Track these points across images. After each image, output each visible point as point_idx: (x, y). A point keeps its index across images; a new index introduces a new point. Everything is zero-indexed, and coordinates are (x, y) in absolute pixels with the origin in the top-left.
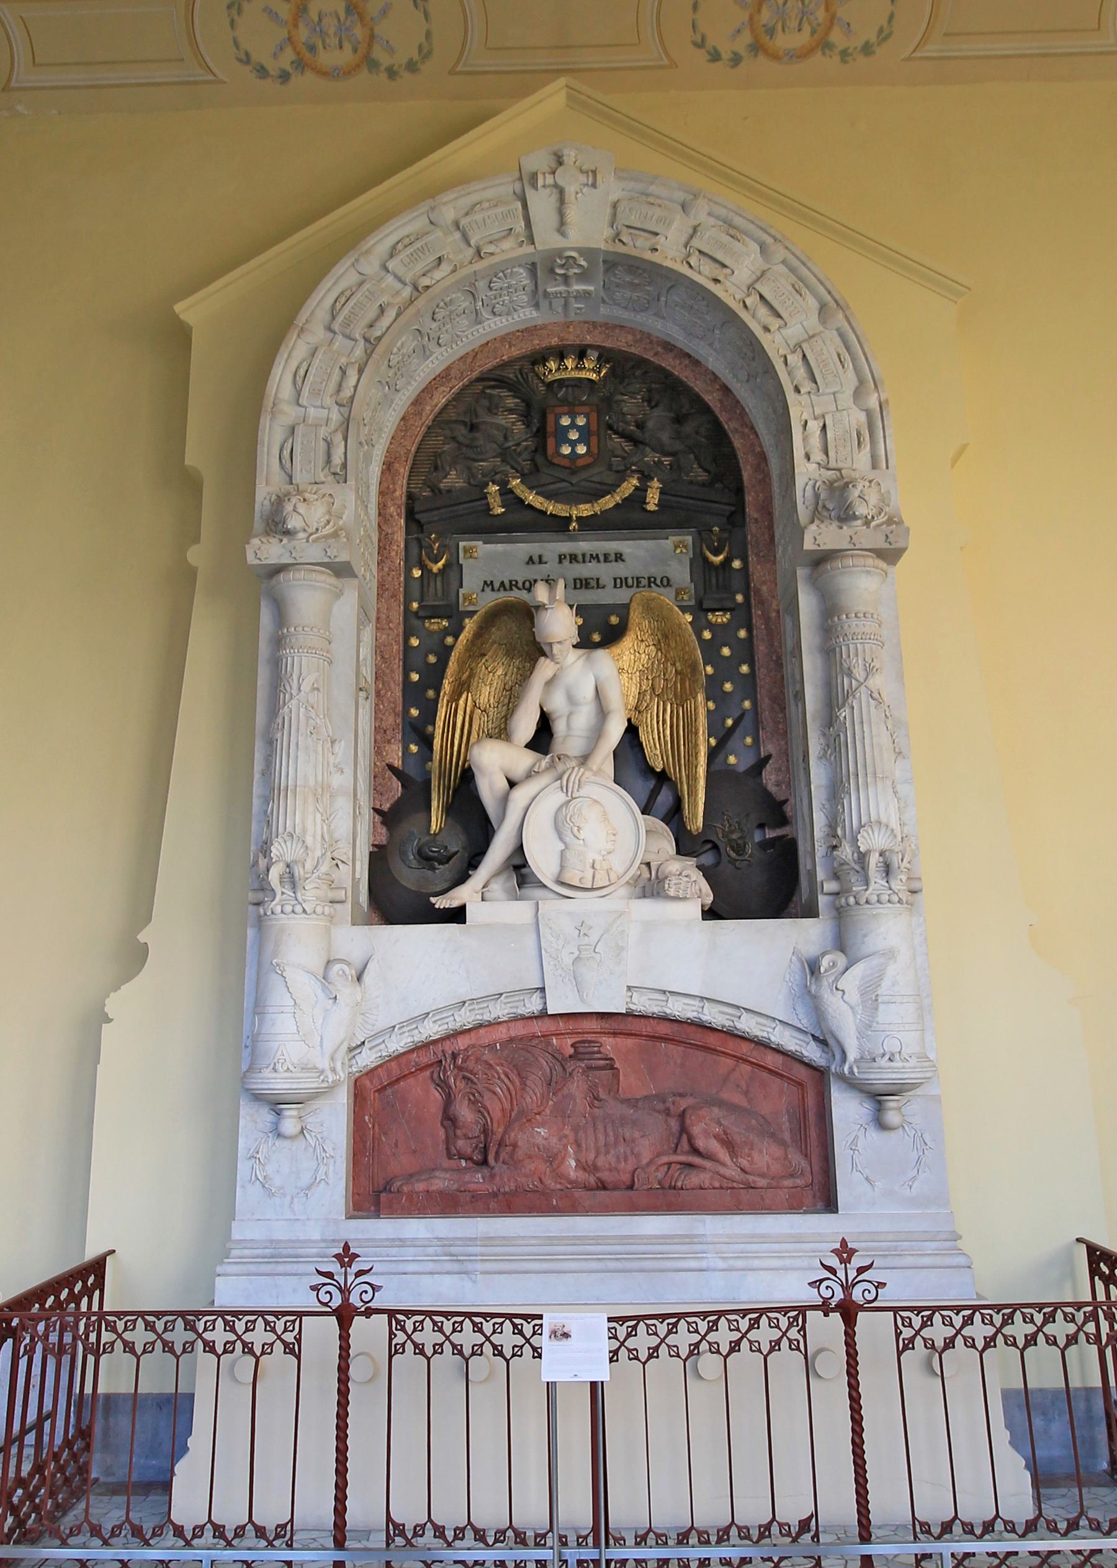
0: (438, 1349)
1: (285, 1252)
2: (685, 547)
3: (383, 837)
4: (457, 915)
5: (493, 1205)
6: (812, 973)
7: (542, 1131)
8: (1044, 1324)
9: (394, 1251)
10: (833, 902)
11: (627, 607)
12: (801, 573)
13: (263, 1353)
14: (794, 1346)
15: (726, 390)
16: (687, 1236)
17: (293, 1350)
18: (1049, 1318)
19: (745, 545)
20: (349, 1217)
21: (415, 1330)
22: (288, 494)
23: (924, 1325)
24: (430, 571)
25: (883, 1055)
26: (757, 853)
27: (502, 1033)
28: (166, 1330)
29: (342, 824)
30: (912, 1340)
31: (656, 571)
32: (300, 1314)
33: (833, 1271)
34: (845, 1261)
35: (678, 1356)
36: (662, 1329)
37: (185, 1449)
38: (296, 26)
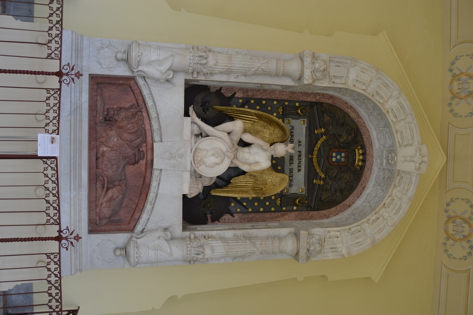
0: (48, 105)
1: (79, 53)
2: (302, 192)
3: (213, 90)
4: (187, 114)
5: (92, 123)
6: (165, 229)
7: (115, 140)
8: (55, 299)
9: (78, 89)
10: (187, 237)
11: (283, 172)
12: (292, 230)
13: (48, 47)
14: (48, 221)
15: (350, 206)
16: (81, 186)
17: (49, 56)
18: (57, 300)
19: (300, 211)
20: (90, 75)
21: (54, 97)
22: (50, 3)
23: (55, 262)
24: (298, 109)
25: (138, 251)
26: (201, 209)
27: (147, 127)
28: (57, 14)
29: (217, 78)
30: (50, 258)
31: (294, 182)
32: (60, 59)
33: (71, 234)
34: (75, 238)
35: (45, 184)
36: (54, 179)
37: (17, 19)
38: (466, 75)
